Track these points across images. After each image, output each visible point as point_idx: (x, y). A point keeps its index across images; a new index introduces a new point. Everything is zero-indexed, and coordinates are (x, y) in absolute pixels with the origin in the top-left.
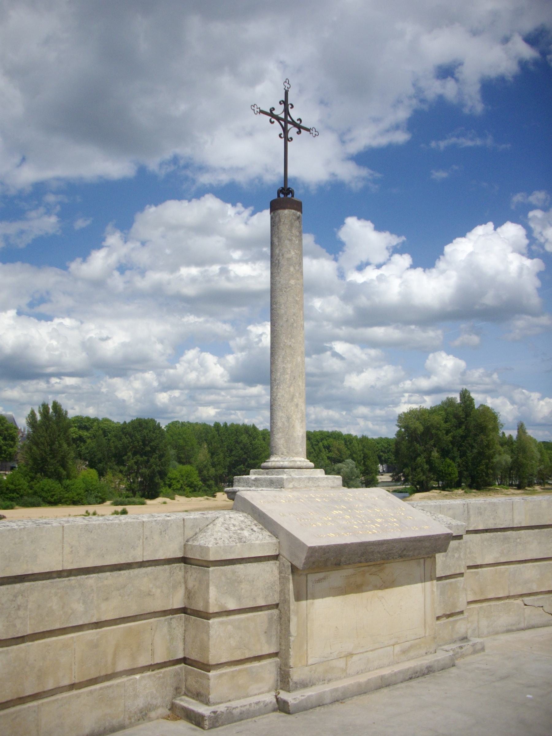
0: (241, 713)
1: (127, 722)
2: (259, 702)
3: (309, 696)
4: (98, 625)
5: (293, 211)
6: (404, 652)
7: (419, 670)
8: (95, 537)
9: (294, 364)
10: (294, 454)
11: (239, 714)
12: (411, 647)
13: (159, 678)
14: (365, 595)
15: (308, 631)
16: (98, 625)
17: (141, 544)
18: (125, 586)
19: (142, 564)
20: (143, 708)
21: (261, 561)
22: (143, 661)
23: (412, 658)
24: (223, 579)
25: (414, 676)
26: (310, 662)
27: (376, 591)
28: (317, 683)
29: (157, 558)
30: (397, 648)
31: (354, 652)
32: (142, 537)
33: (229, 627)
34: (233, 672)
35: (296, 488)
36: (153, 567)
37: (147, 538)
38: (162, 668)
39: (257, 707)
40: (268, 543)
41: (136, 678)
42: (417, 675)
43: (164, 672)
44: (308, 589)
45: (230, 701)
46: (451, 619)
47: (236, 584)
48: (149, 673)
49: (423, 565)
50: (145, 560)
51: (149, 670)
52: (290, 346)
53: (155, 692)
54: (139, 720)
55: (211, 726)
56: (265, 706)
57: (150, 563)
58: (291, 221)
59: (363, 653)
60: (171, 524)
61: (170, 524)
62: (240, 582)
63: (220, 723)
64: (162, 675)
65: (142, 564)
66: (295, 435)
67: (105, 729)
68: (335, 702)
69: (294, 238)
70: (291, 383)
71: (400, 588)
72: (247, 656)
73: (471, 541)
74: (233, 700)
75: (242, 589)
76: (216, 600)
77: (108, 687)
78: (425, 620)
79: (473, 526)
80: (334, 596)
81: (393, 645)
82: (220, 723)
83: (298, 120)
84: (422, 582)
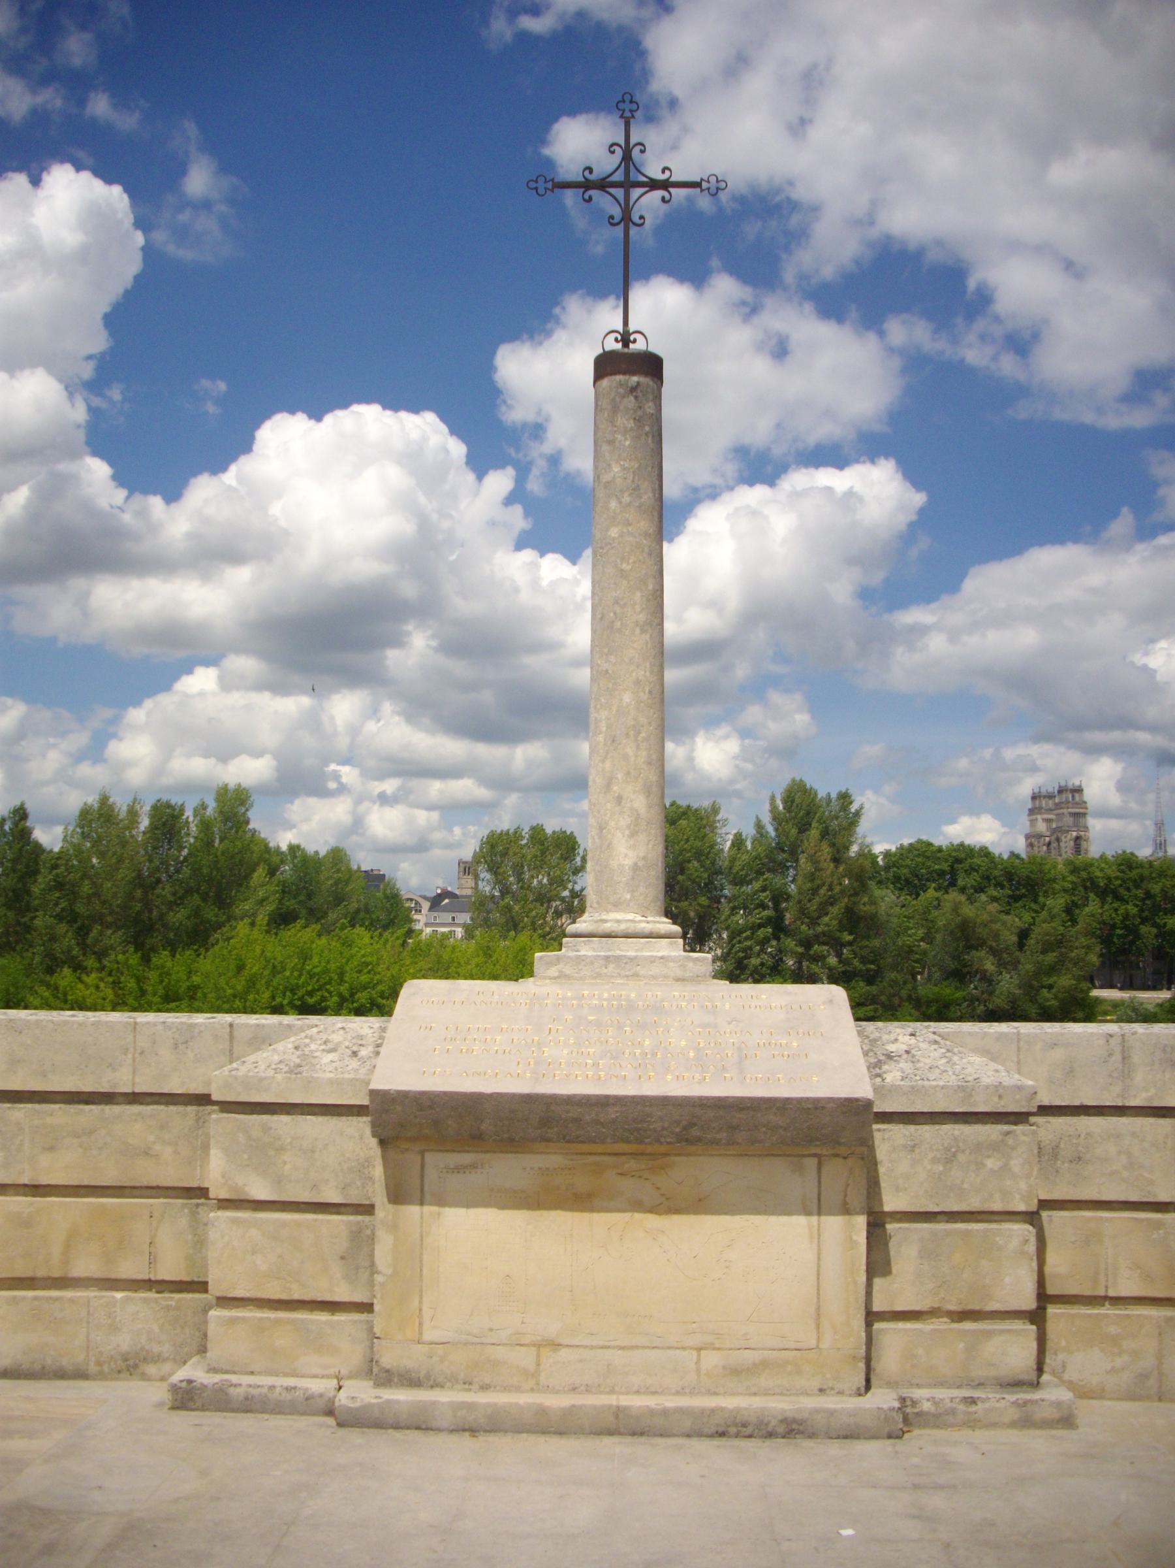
0: (247, 1399)
1: (93, 1368)
2: (295, 1388)
3: (388, 1401)
4: (36, 1190)
5: (619, 378)
6: (735, 1372)
7: (754, 1420)
8: (29, 1042)
9: (614, 709)
10: (610, 907)
11: (241, 1398)
12: (765, 1365)
13: (168, 1308)
14: (597, 1217)
15: (425, 1271)
16: (36, 1190)
17: (129, 1061)
18: (91, 1132)
19: (134, 1098)
20: (128, 1353)
21: (340, 1115)
22: (129, 1269)
23: (767, 1393)
24: (241, 1137)
25: (733, 1430)
26: (428, 1336)
27: (637, 1216)
28: (448, 1384)
29: (166, 1091)
30: (711, 1360)
31: (565, 1341)
32: (132, 1050)
33: (254, 1232)
34: (261, 1319)
35: (568, 977)
36: (162, 1107)
37: (142, 1053)
38: (180, 1291)
39: (287, 1397)
40: (352, 1080)
41: (113, 1297)
42: (749, 1430)
43: (179, 1300)
44: (426, 1181)
45: (252, 1373)
46: (968, 1325)
47: (271, 1153)
48: (152, 1295)
49: (814, 1173)
50: (137, 1091)
51: (150, 1290)
52: (607, 671)
53: (157, 1330)
54: (119, 1372)
55: (178, 1404)
56: (307, 1399)
57: (156, 1098)
58: (613, 400)
59: (592, 1348)
60: (201, 1032)
61: (197, 1030)
62: (282, 1149)
63: (199, 1404)
64: (173, 1303)
65: (134, 1098)
66: (614, 864)
67: (43, 1368)
68: (464, 1430)
69: (619, 437)
70: (607, 753)
71: (727, 1218)
72: (296, 1296)
73: (1134, 1134)
74: (260, 1373)
75: (285, 1163)
76: (223, 1177)
77: (57, 1299)
78: (818, 1308)
79: (1144, 1095)
80: (503, 1207)
81: (699, 1350)
82: (199, 1404)
83: (663, 172)
84: (807, 1213)
